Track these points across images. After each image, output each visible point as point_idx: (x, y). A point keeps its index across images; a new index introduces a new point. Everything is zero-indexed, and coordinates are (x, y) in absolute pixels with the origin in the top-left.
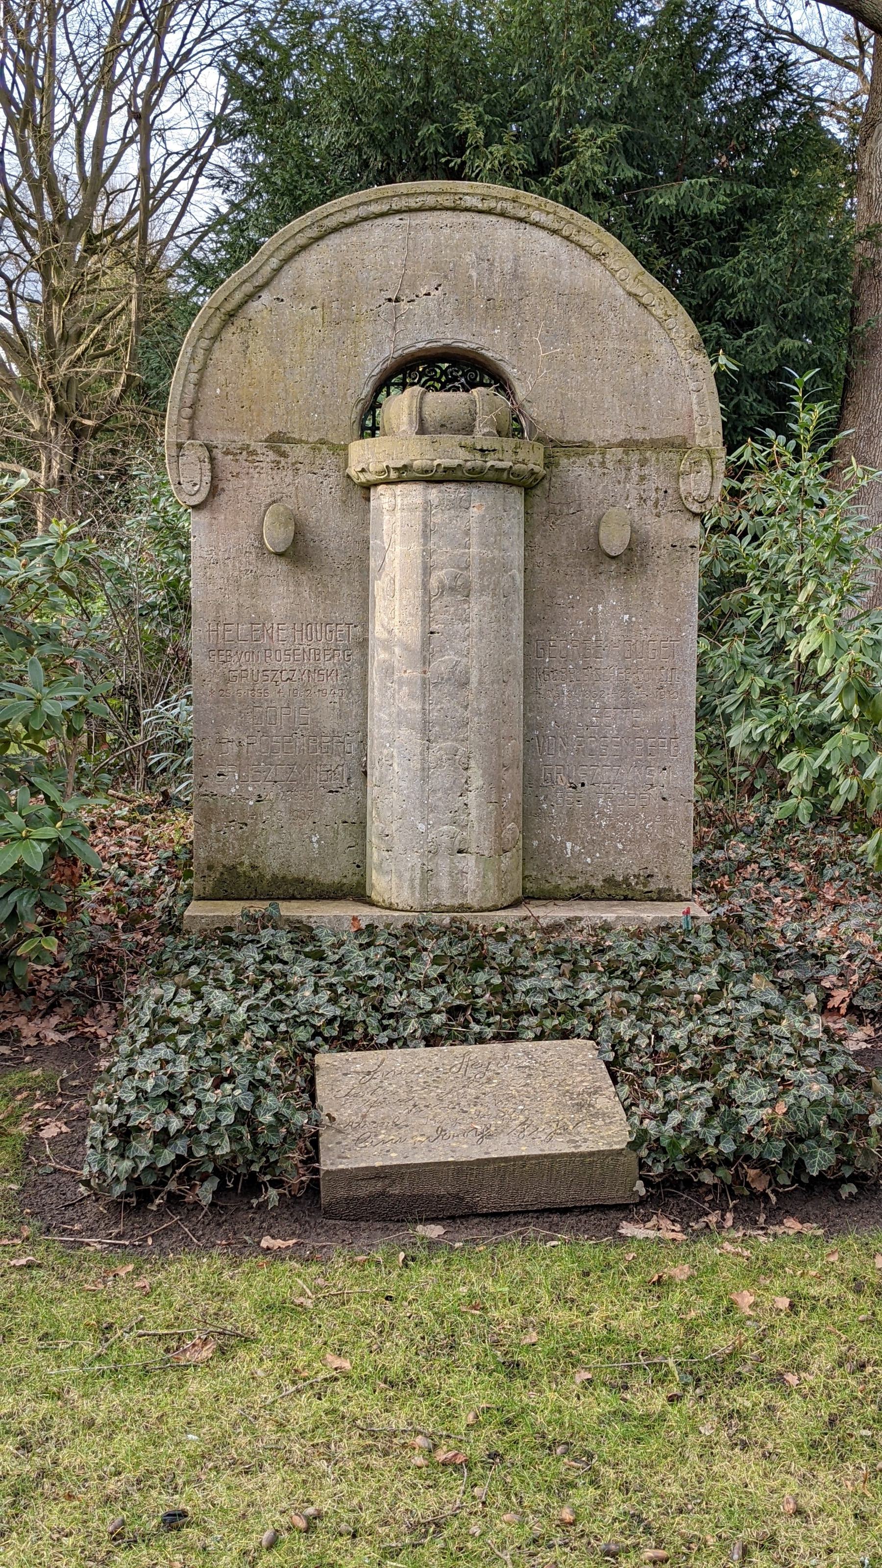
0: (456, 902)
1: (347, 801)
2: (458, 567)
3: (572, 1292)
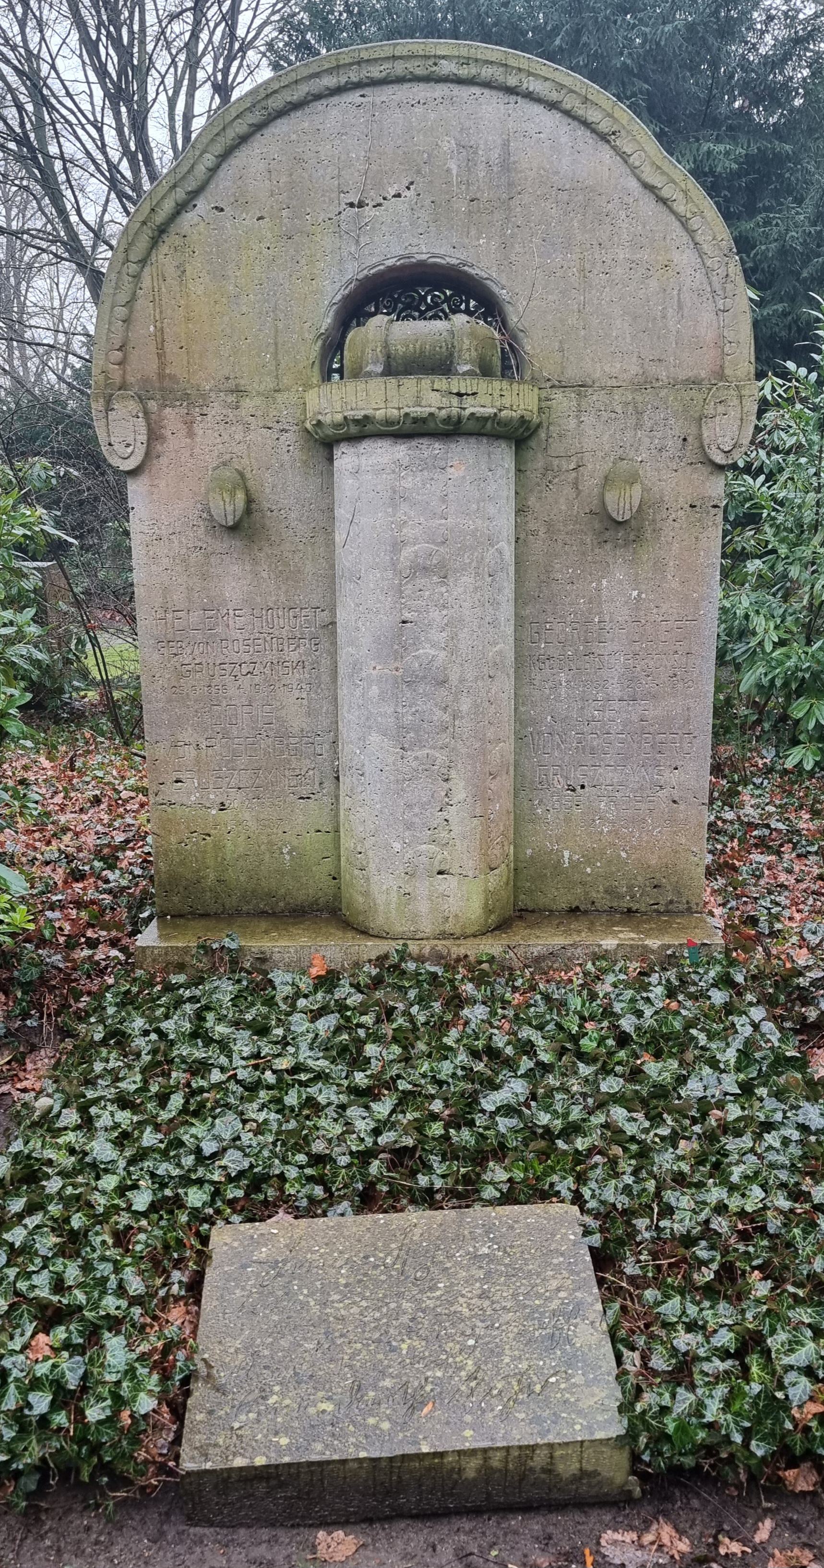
2: (434, 542)
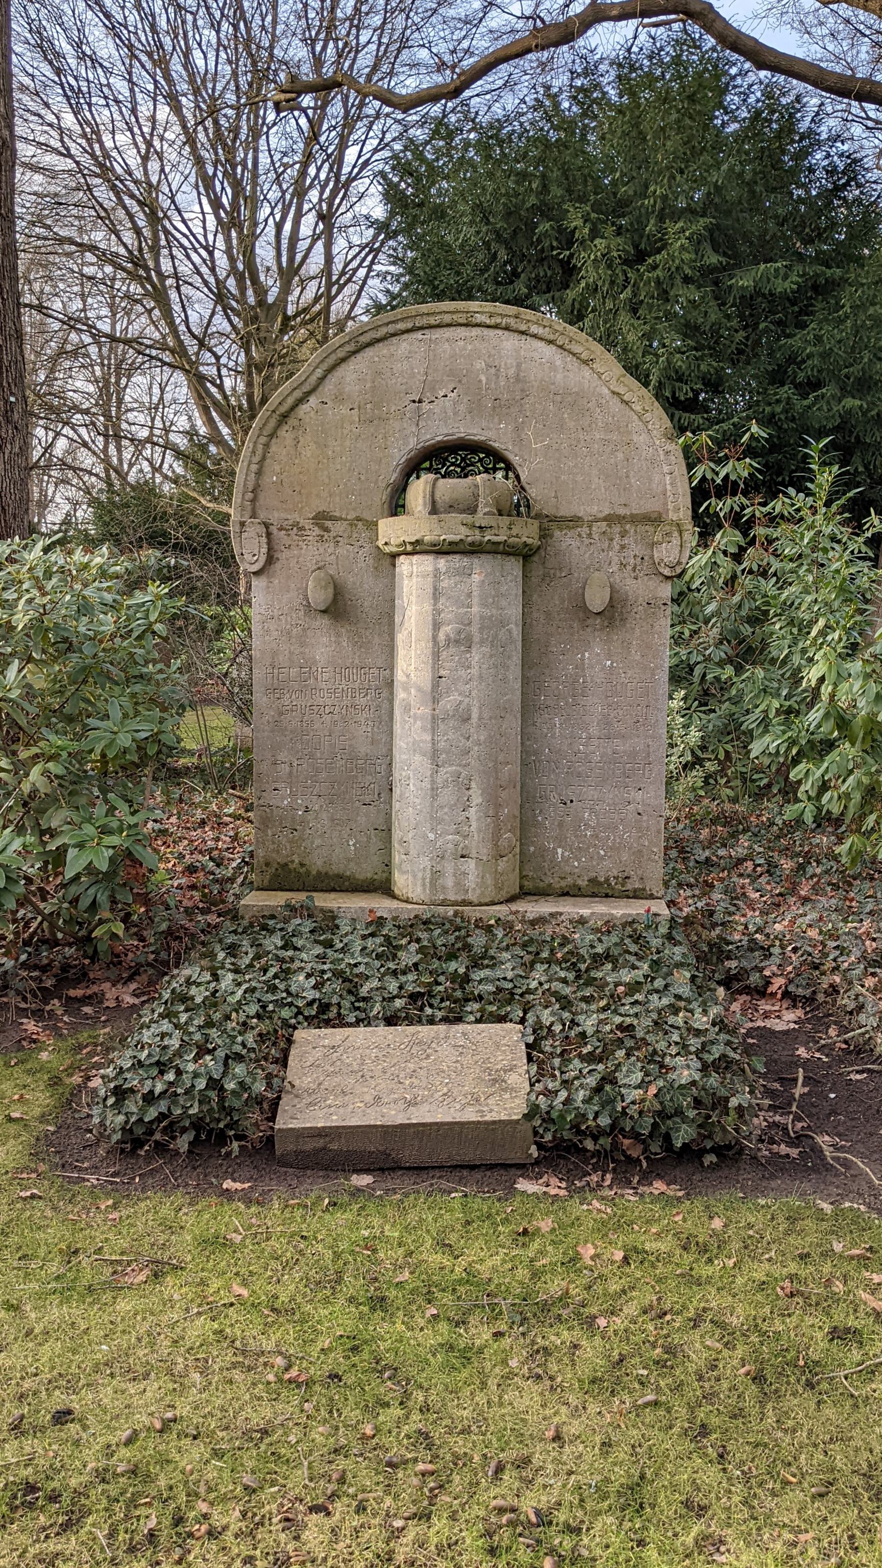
0: (459, 898)
1: (378, 811)
3: (452, 1238)
